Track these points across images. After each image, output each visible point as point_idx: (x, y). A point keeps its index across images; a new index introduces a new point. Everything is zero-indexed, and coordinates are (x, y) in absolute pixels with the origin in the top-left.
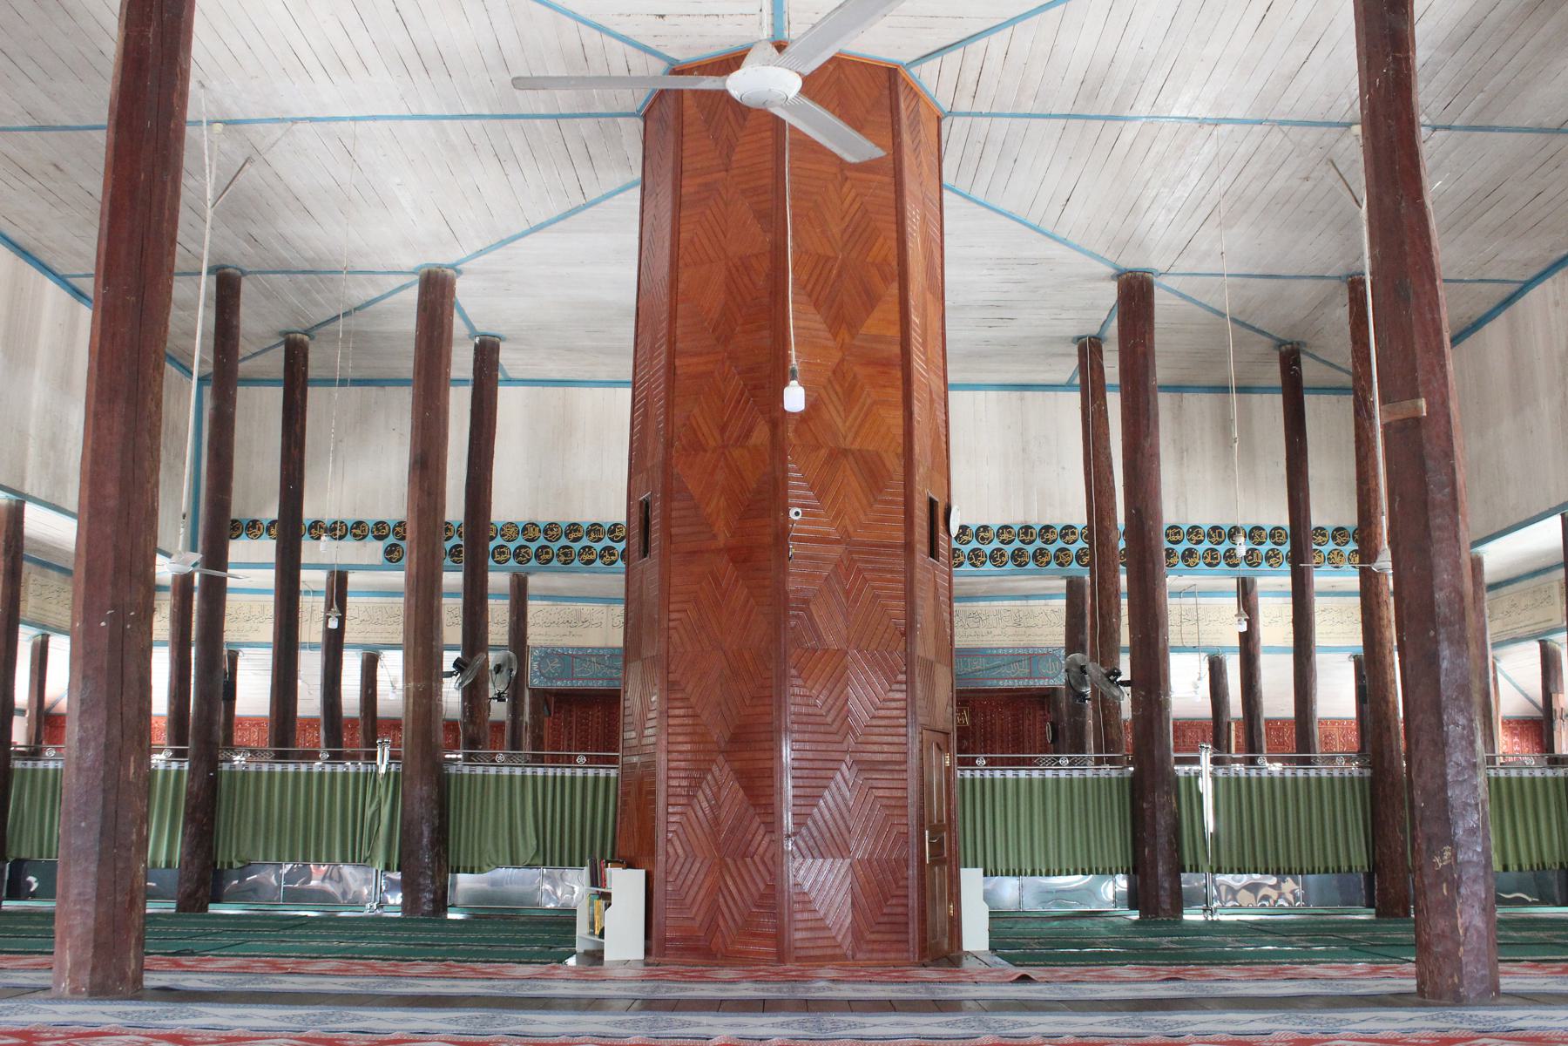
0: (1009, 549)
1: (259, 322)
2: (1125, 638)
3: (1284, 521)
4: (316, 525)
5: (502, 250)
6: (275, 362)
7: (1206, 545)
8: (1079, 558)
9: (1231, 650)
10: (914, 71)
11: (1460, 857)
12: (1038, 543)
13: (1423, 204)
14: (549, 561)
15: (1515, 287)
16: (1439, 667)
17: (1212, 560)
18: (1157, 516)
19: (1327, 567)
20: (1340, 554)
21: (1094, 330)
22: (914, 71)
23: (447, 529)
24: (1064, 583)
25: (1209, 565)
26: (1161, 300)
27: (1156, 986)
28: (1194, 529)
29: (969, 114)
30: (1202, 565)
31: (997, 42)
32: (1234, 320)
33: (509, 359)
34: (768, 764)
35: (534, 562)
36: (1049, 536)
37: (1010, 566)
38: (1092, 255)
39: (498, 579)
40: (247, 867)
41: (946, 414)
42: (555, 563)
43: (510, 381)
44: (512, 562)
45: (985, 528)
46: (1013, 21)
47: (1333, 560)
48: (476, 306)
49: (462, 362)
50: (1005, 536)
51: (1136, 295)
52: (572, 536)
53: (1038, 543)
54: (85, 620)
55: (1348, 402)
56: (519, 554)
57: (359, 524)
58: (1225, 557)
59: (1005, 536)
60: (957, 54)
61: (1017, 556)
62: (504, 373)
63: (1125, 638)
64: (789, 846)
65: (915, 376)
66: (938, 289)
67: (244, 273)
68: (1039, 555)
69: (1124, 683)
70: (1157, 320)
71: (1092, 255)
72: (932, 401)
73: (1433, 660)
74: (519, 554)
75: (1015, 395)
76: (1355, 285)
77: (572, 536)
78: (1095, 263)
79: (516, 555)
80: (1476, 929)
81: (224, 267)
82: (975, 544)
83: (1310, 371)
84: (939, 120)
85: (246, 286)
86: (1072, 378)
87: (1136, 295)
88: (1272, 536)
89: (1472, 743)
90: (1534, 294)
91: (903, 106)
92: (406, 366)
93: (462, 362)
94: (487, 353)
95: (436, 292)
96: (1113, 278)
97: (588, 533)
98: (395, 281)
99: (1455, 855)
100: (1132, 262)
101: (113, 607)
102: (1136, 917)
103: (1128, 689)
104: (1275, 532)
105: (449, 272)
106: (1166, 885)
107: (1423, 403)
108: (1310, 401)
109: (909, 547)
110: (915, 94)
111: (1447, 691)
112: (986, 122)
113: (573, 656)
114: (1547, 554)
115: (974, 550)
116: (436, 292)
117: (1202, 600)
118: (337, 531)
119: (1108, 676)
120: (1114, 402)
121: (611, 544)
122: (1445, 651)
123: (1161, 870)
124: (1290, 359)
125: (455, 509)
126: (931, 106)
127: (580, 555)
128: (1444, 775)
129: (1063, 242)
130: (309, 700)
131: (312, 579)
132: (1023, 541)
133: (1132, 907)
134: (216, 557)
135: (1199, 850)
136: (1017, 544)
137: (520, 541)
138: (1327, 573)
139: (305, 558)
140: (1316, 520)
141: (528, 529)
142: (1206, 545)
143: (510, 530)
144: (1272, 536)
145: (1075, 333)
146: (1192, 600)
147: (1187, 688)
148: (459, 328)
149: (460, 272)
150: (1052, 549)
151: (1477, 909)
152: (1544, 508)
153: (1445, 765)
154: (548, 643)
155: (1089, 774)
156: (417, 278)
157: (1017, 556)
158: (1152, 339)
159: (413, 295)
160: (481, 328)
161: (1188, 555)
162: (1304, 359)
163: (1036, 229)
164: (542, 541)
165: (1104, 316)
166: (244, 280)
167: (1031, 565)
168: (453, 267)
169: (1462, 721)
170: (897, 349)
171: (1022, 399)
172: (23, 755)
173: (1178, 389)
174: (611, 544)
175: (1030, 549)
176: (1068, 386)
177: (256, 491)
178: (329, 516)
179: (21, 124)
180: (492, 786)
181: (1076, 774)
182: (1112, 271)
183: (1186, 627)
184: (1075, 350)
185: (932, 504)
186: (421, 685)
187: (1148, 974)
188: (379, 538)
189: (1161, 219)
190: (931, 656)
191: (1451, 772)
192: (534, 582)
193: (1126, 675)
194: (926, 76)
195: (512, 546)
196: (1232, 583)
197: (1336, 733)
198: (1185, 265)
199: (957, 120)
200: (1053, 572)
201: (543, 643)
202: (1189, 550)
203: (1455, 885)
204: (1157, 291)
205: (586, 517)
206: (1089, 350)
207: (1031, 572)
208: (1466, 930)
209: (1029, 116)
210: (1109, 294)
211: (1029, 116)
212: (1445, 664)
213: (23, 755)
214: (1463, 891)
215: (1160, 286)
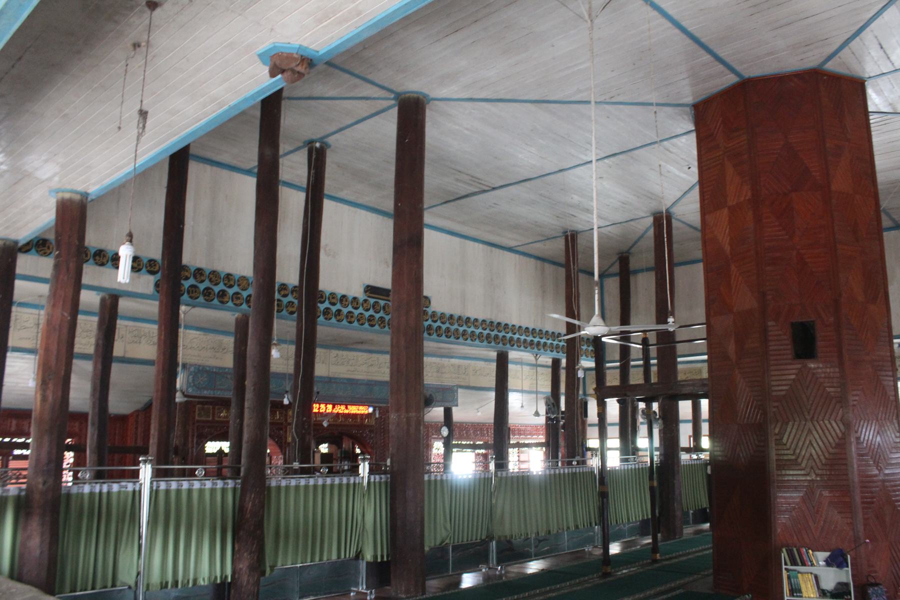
8: (248, 301)
23: (322, 297)
40: (506, 537)
52: (282, 293)
58: (347, 317)
68: (207, 292)
77: (282, 293)
79: (369, 320)
83: (633, 264)
97: (292, 292)
113: (216, 373)
121: (224, 288)
125: (288, 271)
127: (287, 307)
130: (80, 394)
132: (225, 284)
139: (85, 280)
154: (200, 362)
157: (360, 319)
171: (491, 251)
172: (688, 450)
174: (224, 288)
175: (231, 292)
180: (433, 487)
188: (152, 273)
192: (513, 355)
196: (494, 354)
200: (492, 347)
201: (196, 362)
205: (340, 291)
213: (688, 450)
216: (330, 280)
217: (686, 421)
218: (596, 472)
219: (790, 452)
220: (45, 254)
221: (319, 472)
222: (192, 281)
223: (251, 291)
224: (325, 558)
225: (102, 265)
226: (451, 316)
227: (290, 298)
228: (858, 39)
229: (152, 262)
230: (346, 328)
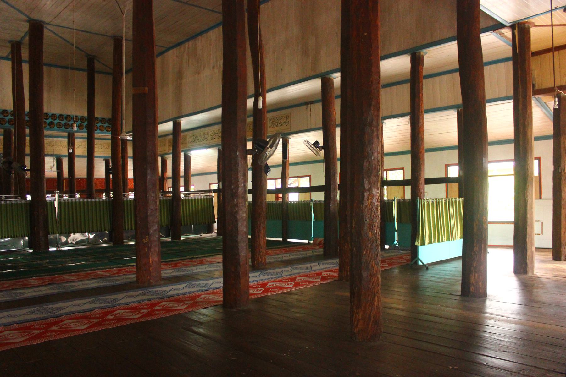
2: (28, 150)
3: (86, 115)
7: (57, 121)
9: (65, 156)
13: (152, 19)
15: (164, 49)
16: (147, 177)
17: (59, 126)
19: (98, 131)
20: (103, 127)
21: (19, 39)
24: (3, 130)
27: (45, 288)
28: (53, 115)
30: (56, 127)
32: (76, 47)
38: (19, 11)
47: (101, 129)
51: (36, 29)
55: (110, 79)
63: (28, 150)
69: (27, 170)
71: (19, 11)
73: (145, 175)
76: (117, 42)
80: (156, 261)
83: (97, 66)
86: (8, 55)
87: (36, 29)
88: (66, 118)
90: (171, 52)
96: (27, 21)
99: (149, 239)
100: (36, 16)
102: (31, 251)
103: (29, 172)
104: (82, 118)
106: (43, 240)
108: (96, 75)
111: (149, 186)
114: (169, 131)
117: (55, 139)
119: (21, 167)
120: (26, 68)
122: (149, 172)
123: (41, 234)
124: (91, 60)
128: (147, 213)
133: (30, 247)
135: (55, 226)
138: (98, 133)
140: (96, 115)
142: (57, 121)
144: (80, 119)
146: (51, 139)
147: (50, 168)
151: (156, 255)
152: (168, 119)
153: (147, 209)
155: (13, 202)
158: (42, 47)
161: (51, 124)
162: (96, 61)
165: (22, 35)
173: (50, 65)
176: (6, 58)
181: (8, 202)
183: (49, 148)
184: (9, 45)
187: (41, 281)
189: (48, 3)
191: (149, 212)
193: (28, 167)
196: (66, 134)
197: (98, 183)
198: (57, 22)
202: (51, 122)
203: (149, 248)
206: (16, 46)
210: (25, 27)
212: (149, 177)
214: (152, 250)
215: (46, 28)
223: (48, 121)
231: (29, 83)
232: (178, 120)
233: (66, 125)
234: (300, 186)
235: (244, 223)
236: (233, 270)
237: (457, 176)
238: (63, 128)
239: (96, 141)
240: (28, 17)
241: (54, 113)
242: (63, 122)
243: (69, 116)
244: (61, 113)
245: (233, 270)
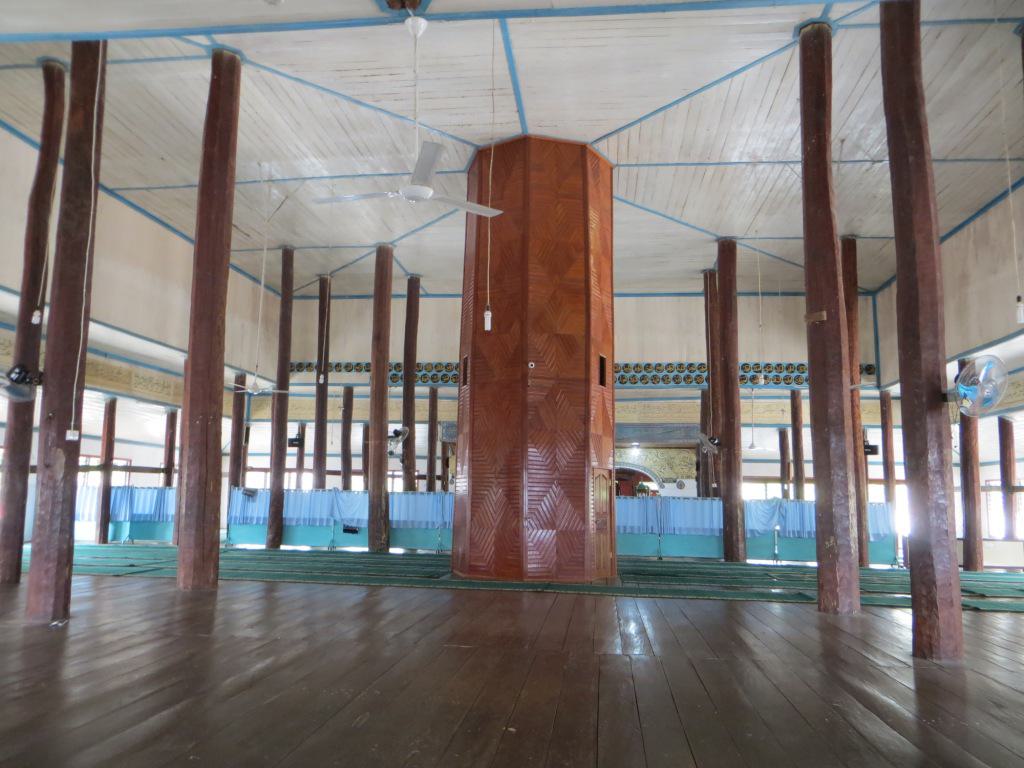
0: (671, 375)
1: (303, 271)
4: (338, 365)
5: (413, 236)
6: (315, 289)
7: (785, 373)
10: (595, 146)
11: (838, 542)
12: (687, 372)
14: (447, 381)
18: (735, 360)
22: (595, 146)
24: (700, 392)
25: (776, 383)
26: (741, 252)
29: (636, 165)
31: (634, 129)
33: (425, 285)
34: (516, 484)
35: (440, 382)
36: (692, 368)
37: (672, 383)
39: (421, 390)
41: (613, 315)
42: (450, 382)
43: (427, 295)
44: (430, 382)
45: (660, 365)
46: (640, 120)
48: (404, 261)
49: (399, 286)
50: (670, 369)
51: (727, 249)
53: (687, 372)
54: (190, 421)
56: (434, 378)
57: (358, 364)
58: (684, 379)
59: (670, 369)
60: (615, 137)
61: (676, 379)
62: (424, 290)
64: (526, 523)
65: (592, 299)
66: (608, 252)
67: (295, 248)
70: (738, 260)
72: (603, 309)
74: (434, 378)
75: (675, 298)
78: (705, 234)
79: (432, 378)
81: (286, 246)
82: (654, 373)
84: (612, 169)
85: (296, 255)
87: (727, 249)
88: (787, 369)
89: (846, 485)
91: (589, 164)
92: (371, 289)
93: (399, 286)
94: (414, 284)
95: (384, 256)
98: (366, 251)
101: (202, 414)
105: (390, 246)
107: (825, 313)
109: (587, 381)
110: (596, 157)
111: (834, 459)
112: (636, 169)
115: (643, 376)
116: (384, 256)
118: (349, 367)
125: (396, 354)
126: (606, 162)
129: (687, 225)
131: (335, 391)
134: (283, 382)
136: (676, 373)
137: (434, 372)
141: (437, 366)
142: (774, 373)
143: (429, 367)
145: (703, 268)
148: (396, 270)
149: (395, 246)
150: (693, 375)
156: (375, 249)
159: (373, 257)
160: (410, 271)
163: (672, 219)
164: (444, 372)
166: (295, 252)
167: (683, 383)
168: (392, 243)
169: (842, 474)
170: (583, 285)
175: (682, 375)
177: (304, 347)
178: (345, 359)
179: (181, 185)
182: (715, 238)
184: (702, 276)
185: (602, 361)
186: (377, 442)
188: (368, 371)
190: (600, 432)
192: (442, 391)
194: (607, 150)
195: (430, 374)
196: (788, 393)
198: (752, 234)
199: (622, 168)
200: (695, 387)
204: (738, 247)
207: (682, 387)
208: (841, 579)
209: (657, 165)
210: (714, 249)
211: (657, 165)
212: (833, 445)
214: (840, 559)
216: (423, 356)
217: (309, 455)
218: (460, 556)
219: (539, 507)
220: (311, 371)
221: (784, 529)
222: (394, 372)
223: (420, 374)
224: (965, 655)
225: (340, 371)
226: (626, 366)
227: (455, 372)
228: (675, 106)
229: (368, 365)
230: (643, 388)
231: (225, 292)
232: (968, 357)
233: (787, 379)
234: (997, 457)
235: (721, 576)
236: (924, 593)
237: (910, 611)
238: (783, 383)
239: (742, 401)
240: (715, 235)
241: (649, 362)
242: (782, 375)
243: (791, 364)
244: (779, 362)
245: (924, 593)
